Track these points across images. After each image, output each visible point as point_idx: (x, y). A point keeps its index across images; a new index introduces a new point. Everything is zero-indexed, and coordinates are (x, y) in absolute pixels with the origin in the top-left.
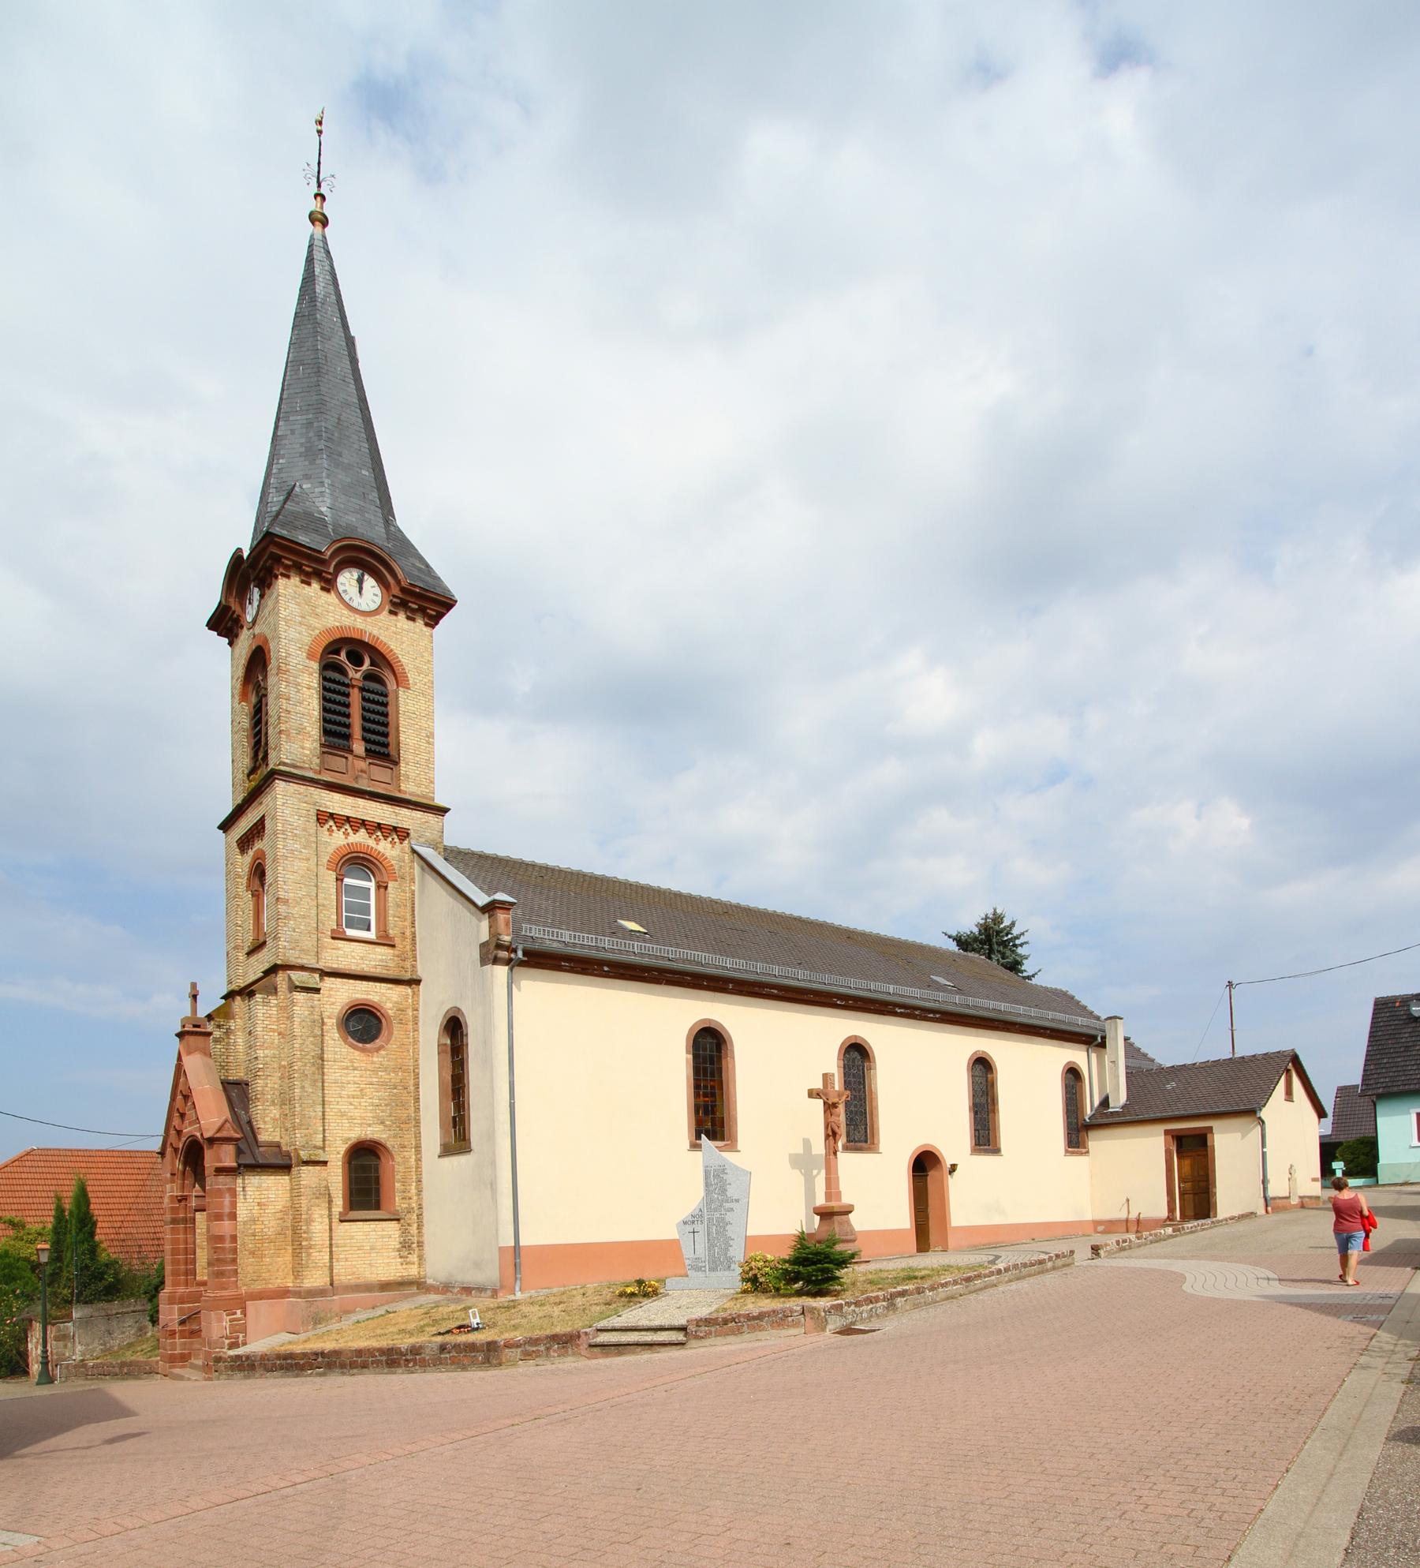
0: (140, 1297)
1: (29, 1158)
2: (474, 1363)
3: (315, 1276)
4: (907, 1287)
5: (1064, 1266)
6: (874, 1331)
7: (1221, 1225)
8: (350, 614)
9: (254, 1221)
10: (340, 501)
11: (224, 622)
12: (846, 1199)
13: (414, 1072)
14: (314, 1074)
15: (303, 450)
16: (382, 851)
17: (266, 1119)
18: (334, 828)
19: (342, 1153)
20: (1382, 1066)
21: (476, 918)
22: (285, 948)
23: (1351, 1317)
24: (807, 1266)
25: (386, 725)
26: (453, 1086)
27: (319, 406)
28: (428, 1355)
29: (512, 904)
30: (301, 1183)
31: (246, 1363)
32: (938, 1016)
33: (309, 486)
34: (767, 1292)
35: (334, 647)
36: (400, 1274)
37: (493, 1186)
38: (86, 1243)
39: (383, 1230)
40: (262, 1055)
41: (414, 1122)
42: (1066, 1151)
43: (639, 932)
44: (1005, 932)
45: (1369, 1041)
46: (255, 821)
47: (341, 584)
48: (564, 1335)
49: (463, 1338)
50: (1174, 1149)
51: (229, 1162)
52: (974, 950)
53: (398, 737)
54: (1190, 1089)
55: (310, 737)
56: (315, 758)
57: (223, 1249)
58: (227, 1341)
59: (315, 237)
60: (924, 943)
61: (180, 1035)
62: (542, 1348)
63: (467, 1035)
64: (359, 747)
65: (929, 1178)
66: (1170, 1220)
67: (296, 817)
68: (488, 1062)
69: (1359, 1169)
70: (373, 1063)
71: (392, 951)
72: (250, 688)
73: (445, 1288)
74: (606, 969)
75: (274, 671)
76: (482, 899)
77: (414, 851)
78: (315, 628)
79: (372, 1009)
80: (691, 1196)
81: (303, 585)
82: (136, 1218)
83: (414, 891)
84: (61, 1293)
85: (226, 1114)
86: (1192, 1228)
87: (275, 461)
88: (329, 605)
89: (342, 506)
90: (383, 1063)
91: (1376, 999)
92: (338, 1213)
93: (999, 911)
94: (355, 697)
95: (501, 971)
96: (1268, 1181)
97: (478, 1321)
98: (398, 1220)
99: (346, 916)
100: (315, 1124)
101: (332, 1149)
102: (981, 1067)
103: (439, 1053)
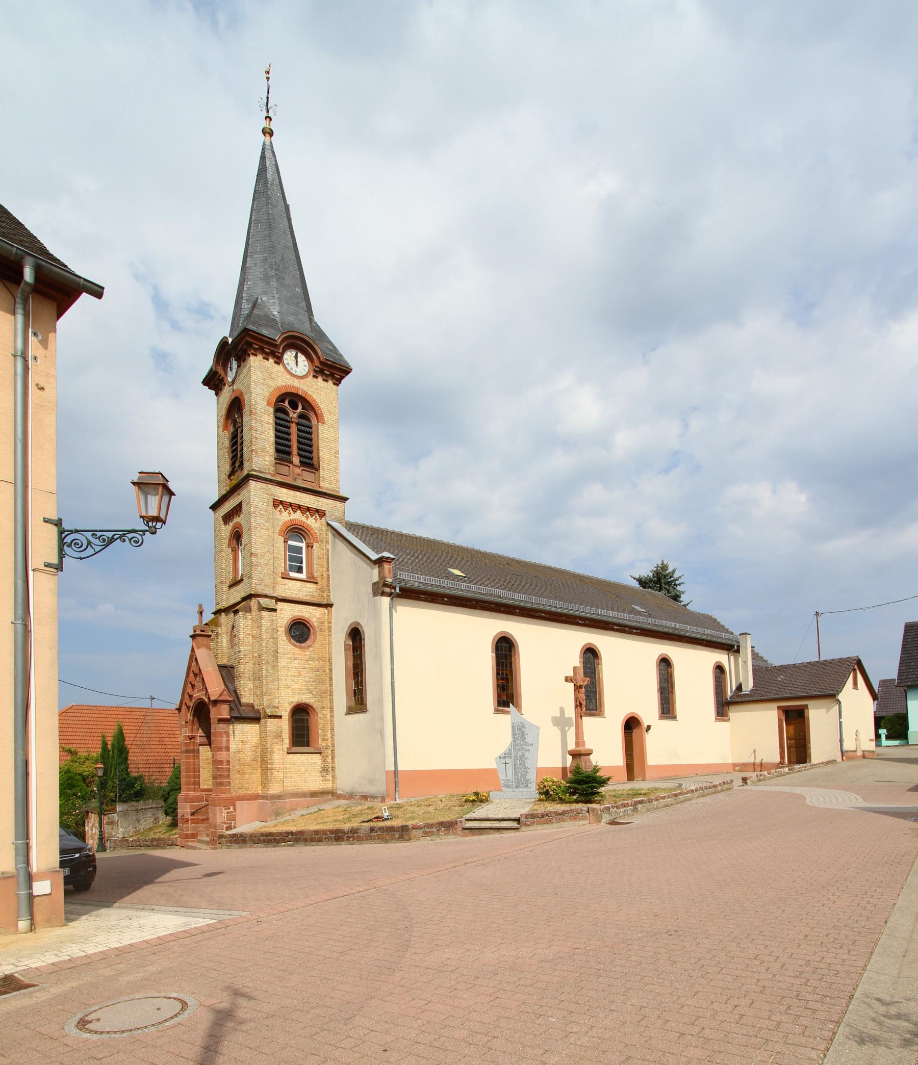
0: (154, 799)
1: (71, 711)
2: (393, 839)
3: (275, 787)
4: (643, 799)
5: (728, 789)
6: (630, 823)
7: (816, 767)
8: (291, 377)
9: (239, 752)
10: (284, 307)
11: (214, 381)
12: (588, 746)
13: (329, 661)
14: (273, 662)
15: (262, 276)
16: (310, 524)
17: (246, 689)
18: (283, 510)
19: (288, 711)
20: (910, 667)
21: (370, 567)
22: (255, 584)
23: (913, 819)
24: (582, 785)
25: (311, 446)
26: (354, 670)
27: (271, 249)
28: (362, 833)
29: (393, 559)
30: (267, 729)
31: (240, 839)
32: (639, 631)
33: (266, 298)
34: (555, 801)
35: (281, 398)
36: (322, 787)
37: (382, 733)
38: (123, 765)
39: (312, 760)
40: (243, 650)
41: (329, 693)
42: (716, 719)
43: (461, 576)
44: (670, 576)
45: (902, 651)
46: (235, 505)
47: (286, 359)
48: (447, 822)
49: (381, 824)
50: (783, 718)
51: (226, 715)
52: (650, 587)
53: (318, 453)
54: (793, 680)
55: (269, 454)
56: (272, 467)
57: (223, 768)
58: (225, 826)
59: (266, 143)
60: (625, 584)
61: (193, 637)
62: (435, 830)
63: (364, 639)
64: (296, 460)
65: (633, 733)
66: (782, 764)
67: (262, 503)
68: (378, 656)
69: (896, 734)
70: (305, 655)
71: (316, 586)
72: (230, 421)
73: (350, 796)
74: (446, 599)
75: (248, 413)
76: (374, 556)
77: (328, 525)
78: (271, 386)
79: (306, 623)
80: (505, 741)
81: (264, 360)
82: (136, 750)
83: (328, 549)
84: (109, 795)
85: (223, 687)
86: (799, 768)
87: (245, 283)
88: (279, 372)
89: (285, 311)
90: (311, 655)
91: (906, 623)
92: (286, 748)
93: (665, 562)
94: (294, 429)
95: (386, 600)
96: (843, 741)
97: (387, 814)
98: (320, 753)
99: (289, 564)
100: (274, 693)
101: (283, 708)
102: (664, 664)
103: (345, 650)
